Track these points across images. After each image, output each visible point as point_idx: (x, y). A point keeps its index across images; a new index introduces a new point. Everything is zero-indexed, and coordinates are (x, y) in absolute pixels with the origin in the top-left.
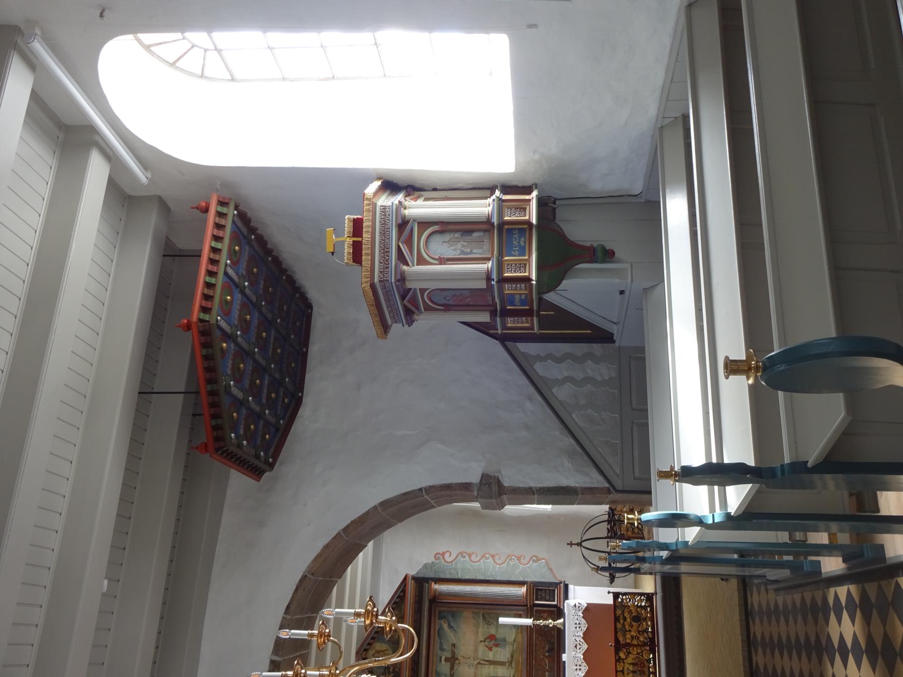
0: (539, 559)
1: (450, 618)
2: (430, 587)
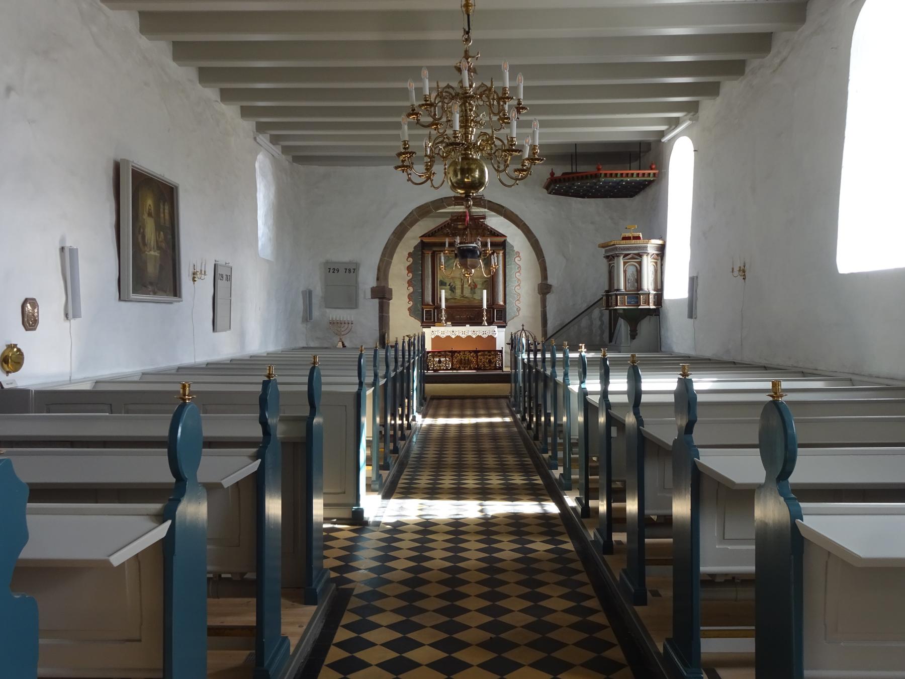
0: (518, 312)
2: (500, 250)
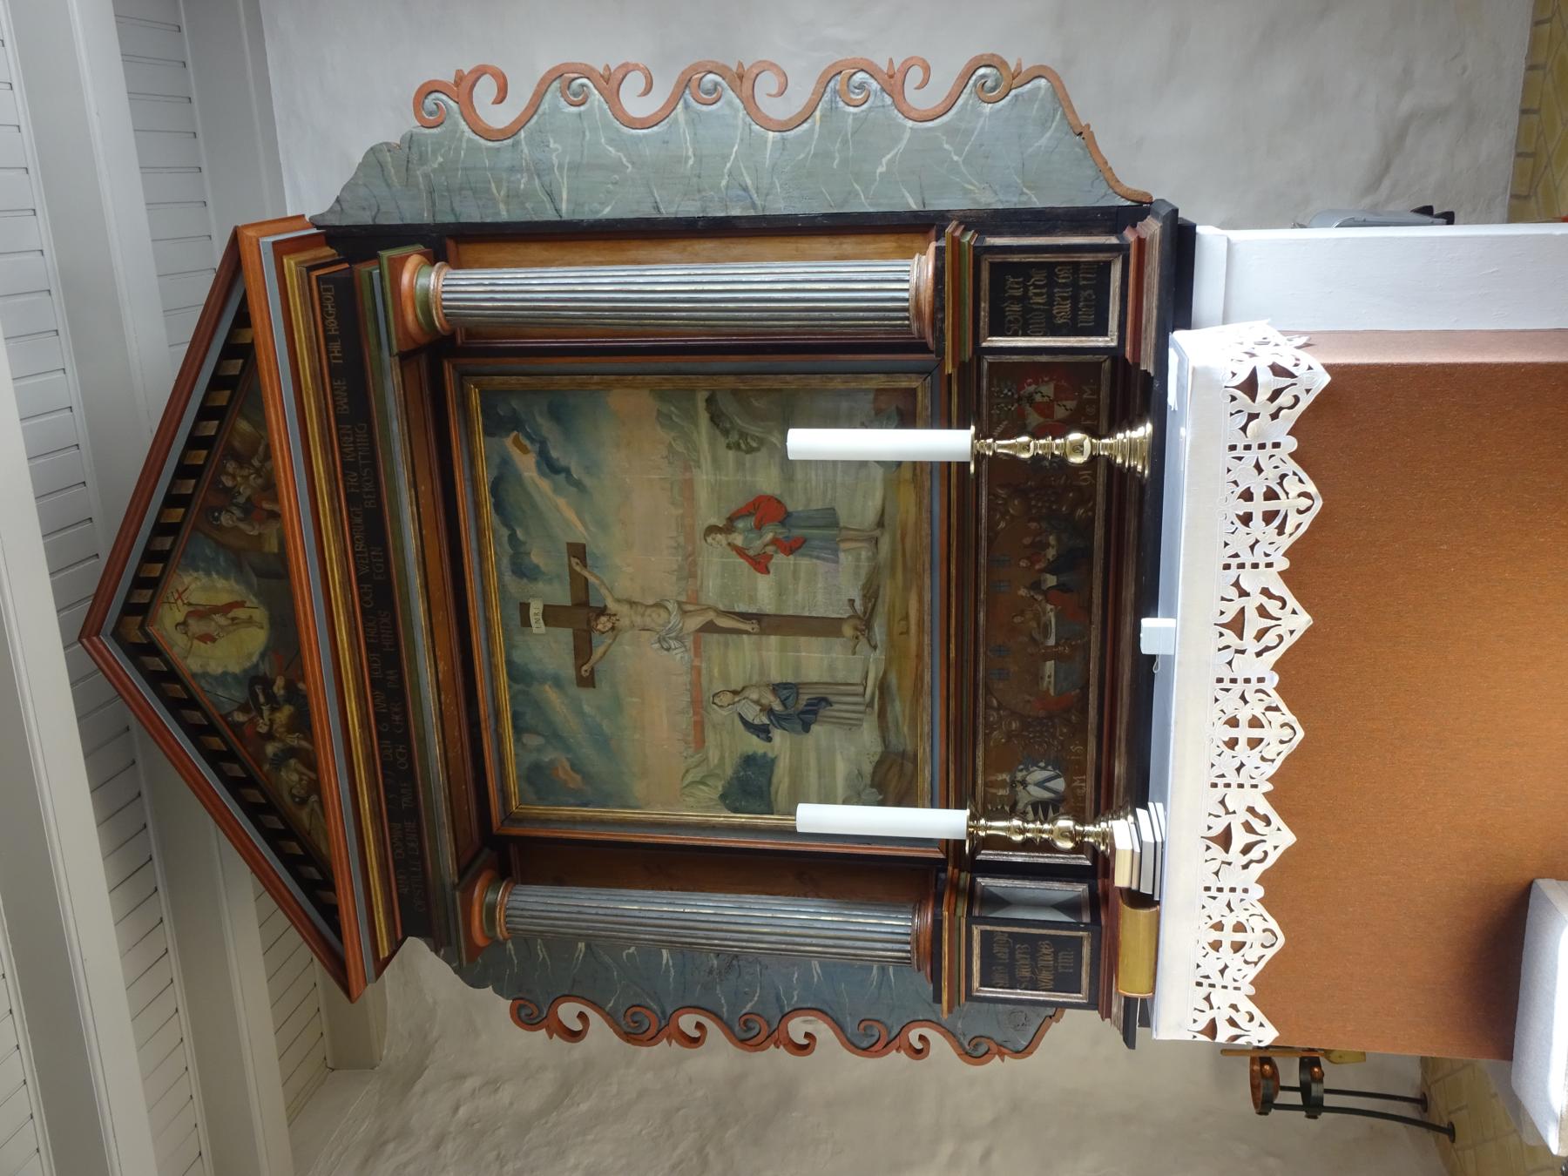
1: (546, 427)
